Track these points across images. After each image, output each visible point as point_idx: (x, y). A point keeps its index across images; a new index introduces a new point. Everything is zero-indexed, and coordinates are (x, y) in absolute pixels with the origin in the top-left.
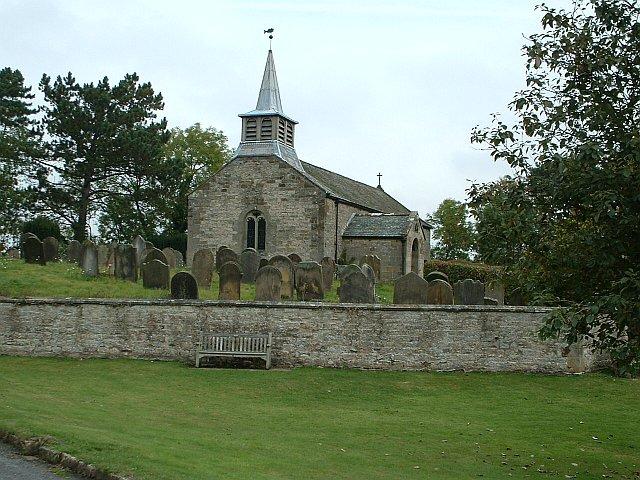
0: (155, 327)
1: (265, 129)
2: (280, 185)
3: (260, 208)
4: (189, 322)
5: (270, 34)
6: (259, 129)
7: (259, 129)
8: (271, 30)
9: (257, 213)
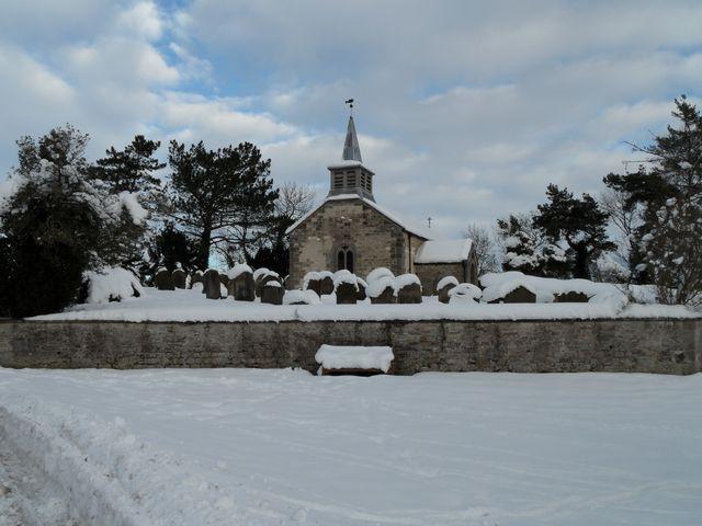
0: (280, 343)
2: (365, 223)
3: (349, 242)
6: (345, 179)
7: (345, 179)
8: (351, 101)
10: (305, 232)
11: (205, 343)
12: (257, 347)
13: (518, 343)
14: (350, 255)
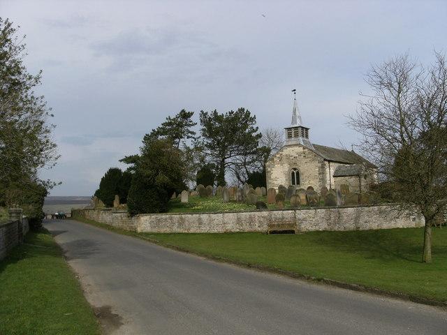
4: (264, 217)
8: (295, 90)
9: (295, 169)
13: (347, 216)
14: (298, 173)
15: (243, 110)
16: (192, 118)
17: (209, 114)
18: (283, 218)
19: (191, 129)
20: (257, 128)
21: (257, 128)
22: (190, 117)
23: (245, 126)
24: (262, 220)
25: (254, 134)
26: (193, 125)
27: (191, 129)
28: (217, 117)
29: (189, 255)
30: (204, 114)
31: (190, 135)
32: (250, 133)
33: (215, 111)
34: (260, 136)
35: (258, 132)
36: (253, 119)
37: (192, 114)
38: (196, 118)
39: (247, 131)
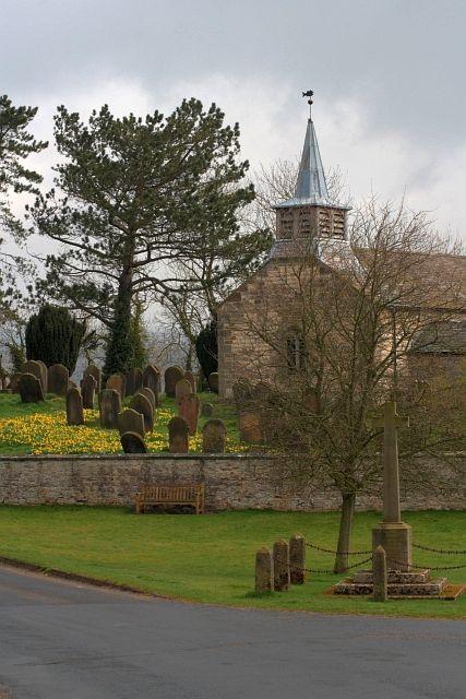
0: (105, 479)
1: (340, 231)
4: (132, 474)
5: (308, 98)
8: (310, 93)
10: (239, 305)
11: (38, 479)
12: (85, 482)
15: (194, 106)
16: (31, 128)
17: (84, 120)
18: (175, 477)
19: (30, 162)
20: (246, 164)
21: (246, 164)
22: (24, 121)
23: (201, 163)
24: (128, 479)
25: (230, 188)
26: (33, 149)
27: (30, 162)
28: (109, 127)
29: (142, 597)
30: (68, 119)
31: (23, 181)
32: (214, 184)
33: (105, 108)
34: (247, 195)
35: (243, 184)
36: (231, 135)
37: (32, 112)
38: (42, 127)
39: (207, 176)
